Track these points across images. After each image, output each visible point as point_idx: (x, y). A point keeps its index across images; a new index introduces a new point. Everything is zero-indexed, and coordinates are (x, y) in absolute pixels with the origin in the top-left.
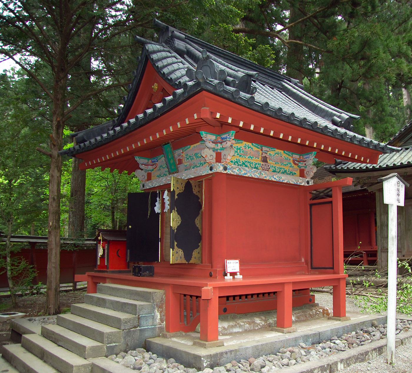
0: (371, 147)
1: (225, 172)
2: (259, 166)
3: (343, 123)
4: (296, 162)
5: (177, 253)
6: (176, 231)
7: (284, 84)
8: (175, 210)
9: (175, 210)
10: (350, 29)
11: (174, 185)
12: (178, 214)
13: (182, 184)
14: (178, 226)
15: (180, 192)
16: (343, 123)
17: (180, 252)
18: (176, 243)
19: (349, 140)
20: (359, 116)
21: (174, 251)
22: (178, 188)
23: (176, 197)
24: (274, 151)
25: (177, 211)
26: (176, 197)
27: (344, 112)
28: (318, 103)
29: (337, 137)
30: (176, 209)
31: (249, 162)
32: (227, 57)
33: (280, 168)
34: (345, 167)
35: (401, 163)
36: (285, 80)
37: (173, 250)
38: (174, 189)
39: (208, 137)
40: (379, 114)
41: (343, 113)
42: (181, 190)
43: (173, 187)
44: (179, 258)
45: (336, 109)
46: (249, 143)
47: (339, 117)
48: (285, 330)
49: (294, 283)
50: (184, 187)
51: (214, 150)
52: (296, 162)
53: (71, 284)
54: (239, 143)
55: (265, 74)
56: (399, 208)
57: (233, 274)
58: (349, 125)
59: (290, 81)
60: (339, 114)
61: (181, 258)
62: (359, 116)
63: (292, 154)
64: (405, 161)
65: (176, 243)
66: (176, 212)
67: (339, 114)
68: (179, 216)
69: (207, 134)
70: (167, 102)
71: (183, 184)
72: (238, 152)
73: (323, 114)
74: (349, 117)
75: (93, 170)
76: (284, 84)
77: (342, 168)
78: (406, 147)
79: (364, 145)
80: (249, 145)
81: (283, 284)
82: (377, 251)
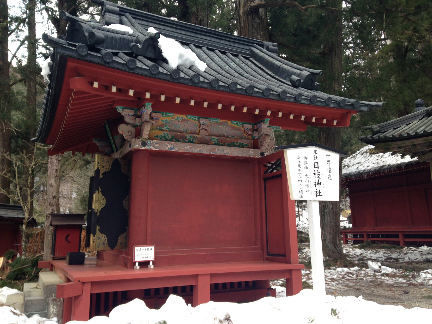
0: (332, 106)
1: (143, 148)
3: (302, 81)
5: (99, 238)
6: (99, 213)
7: (253, 48)
8: (98, 190)
9: (98, 190)
11: (98, 163)
12: (103, 195)
13: (108, 162)
14: (102, 209)
15: (105, 170)
16: (302, 81)
17: (103, 237)
18: (98, 228)
19: (292, 100)
20: (320, 71)
21: (95, 237)
22: (103, 167)
23: (101, 176)
25: (101, 192)
26: (101, 176)
27: (305, 68)
28: (281, 64)
29: (271, 97)
30: (100, 190)
34: (396, 133)
35: (425, 131)
36: (255, 45)
37: (94, 236)
38: (98, 168)
41: (305, 70)
42: (107, 168)
43: (97, 165)
44: (101, 245)
45: (260, 66)
47: (299, 75)
48: (50, 319)
49: (212, 276)
50: (110, 166)
51: (134, 126)
55: (229, 41)
57: (144, 264)
58: (313, 82)
59: (262, 46)
60: (298, 71)
61: (104, 244)
62: (320, 71)
63: (243, 124)
65: (98, 228)
66: (100, 193)
67: (298, 71)
68: (103, 197)
69: (124, 108)
70: (301, 83)
71: (109, 163)
73: (285, 75)
74: (309, 73)
75: (81, 156)
76: (253, 48)
79: (319, 104)
80: (182, 117)
81: (196, 277)
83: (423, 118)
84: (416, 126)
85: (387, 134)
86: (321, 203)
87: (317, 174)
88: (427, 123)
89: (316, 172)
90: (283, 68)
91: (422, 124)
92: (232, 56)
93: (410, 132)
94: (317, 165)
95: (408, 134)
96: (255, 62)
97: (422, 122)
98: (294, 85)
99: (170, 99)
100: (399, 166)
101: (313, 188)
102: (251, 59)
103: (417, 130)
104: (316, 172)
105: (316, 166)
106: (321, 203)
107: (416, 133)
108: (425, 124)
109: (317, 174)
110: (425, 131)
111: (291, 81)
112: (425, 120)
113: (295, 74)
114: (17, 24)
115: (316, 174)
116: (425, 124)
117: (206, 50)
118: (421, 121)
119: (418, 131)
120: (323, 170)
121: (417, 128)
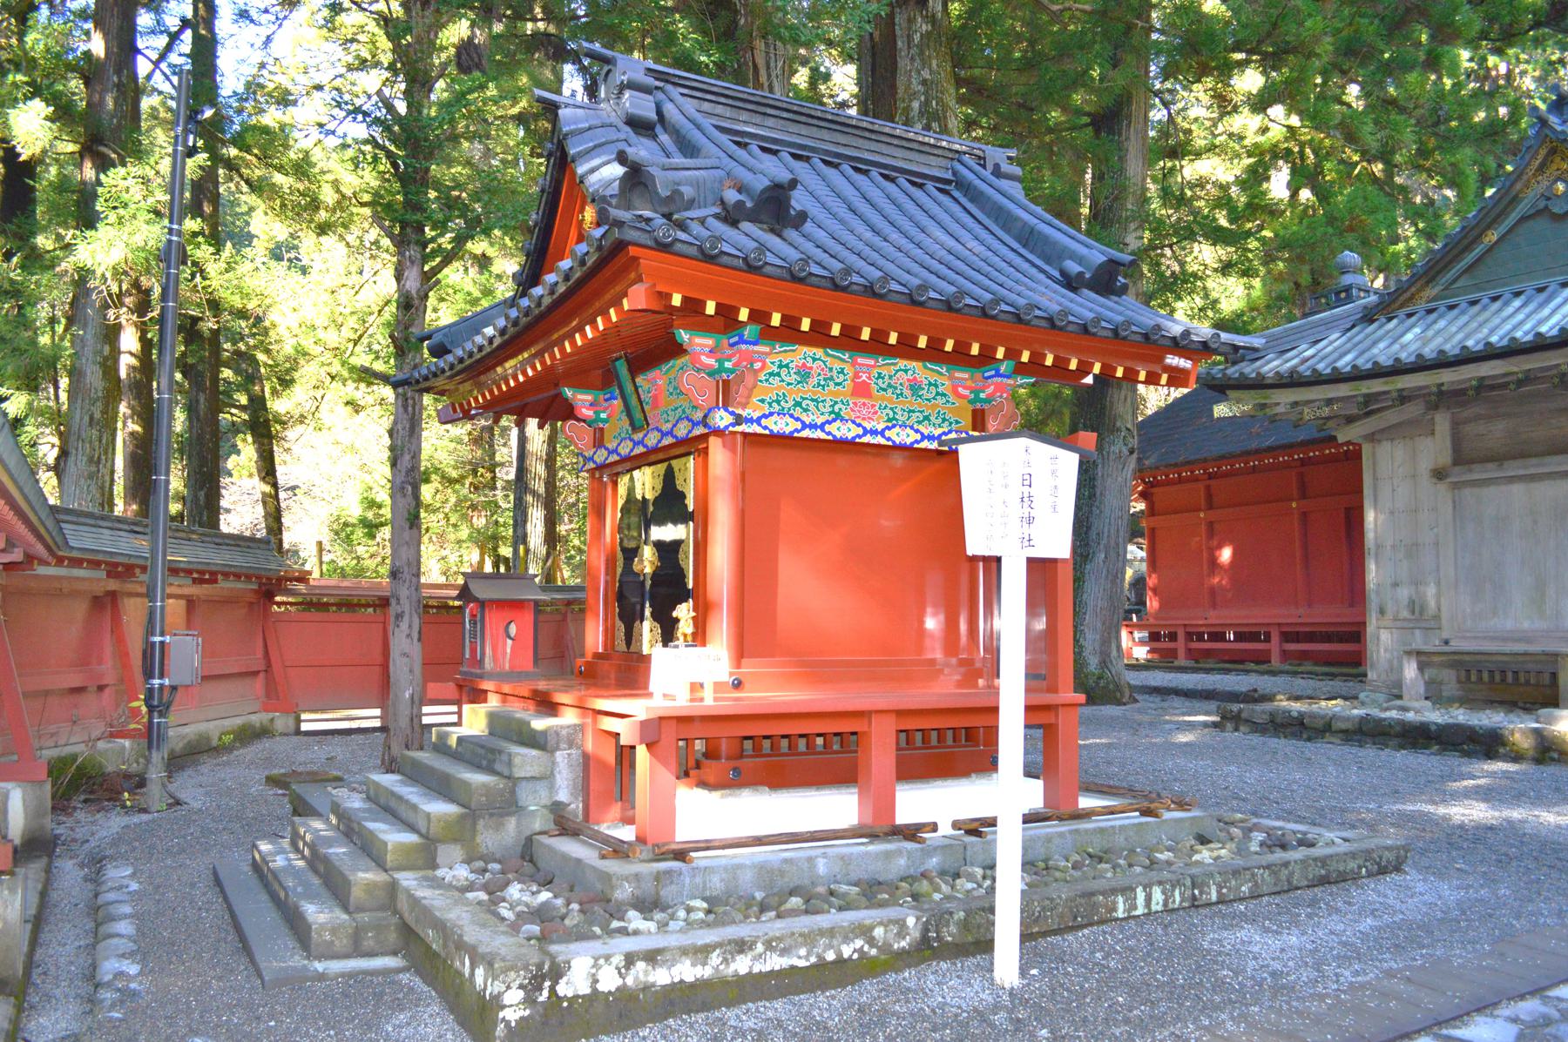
2: (844, 407)
4: (960, 389)
10: (991, 23)
24: (895, 364)
28: (1036, 221)
31: (812, 400)
32: (873, 137)
33: (910, 411)
35: (1355, 367)
39: (698, 342)
40: (202, 360)
46: (814, 350)
52: (960, 389)
53: (377, 712)
54: (785, 351)
56: (1040, 569)
58: (1112, 277)
64: (1549, 328)
72: (783, 374)
77: (1241, 374)
78: (1517, 287)
82: (994, 710)
83: (1353, 326)
84: (1336, 349)
85: (1515, 328)
86: (1033, 563)
87: (1027, 500)
88: (1360, 342)
89: (1026, 495)
90: (1040, 233)
91: (1349, 345)
92: (908, 184)
93: (1320, 366)
94: (1028, 481)
95: (1315, 371)
96: (969, 206)
97: (1350, 339)
98: (1071, 283)
99: (791, 323)
100: (1185, 397)
101: (1016, 530)
102: (956, 194)
103: (1335, 361)
104: (1026, 495)
105: (1027, 482)
106: (1033, 563)
107: (1335, 369)
108: (1356, 345)
109: (1027, 500)
110: (1355, 367)
111: (1063, 273)
112: (1359, 334)
113: (1074, 256)
114: (812, 264)
115: (1026, 499)
116: (1356, 345)
117: (850, 172)
118: (1348, 335)
119: (1339, 364)
120: (1040, 490)
121: (1336, 355)
